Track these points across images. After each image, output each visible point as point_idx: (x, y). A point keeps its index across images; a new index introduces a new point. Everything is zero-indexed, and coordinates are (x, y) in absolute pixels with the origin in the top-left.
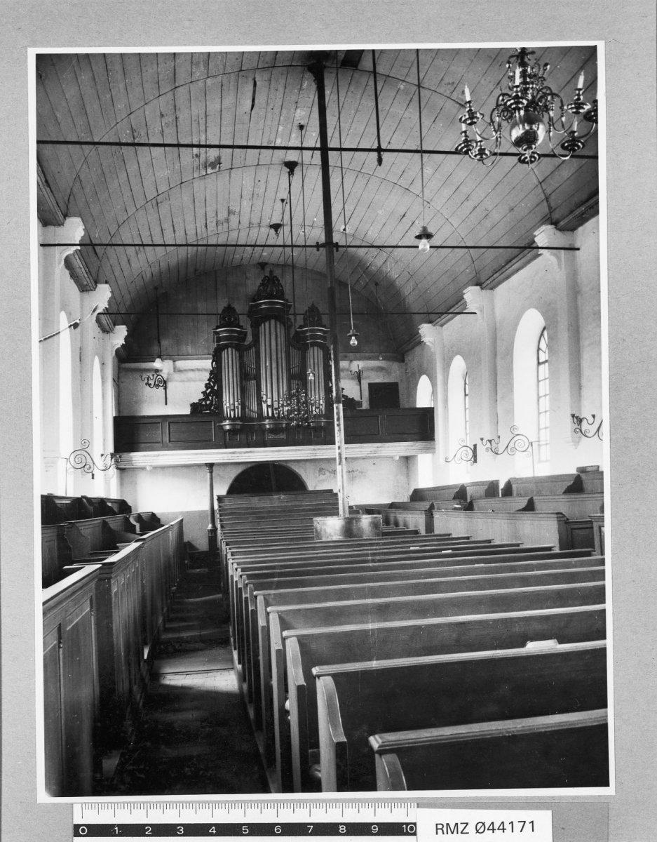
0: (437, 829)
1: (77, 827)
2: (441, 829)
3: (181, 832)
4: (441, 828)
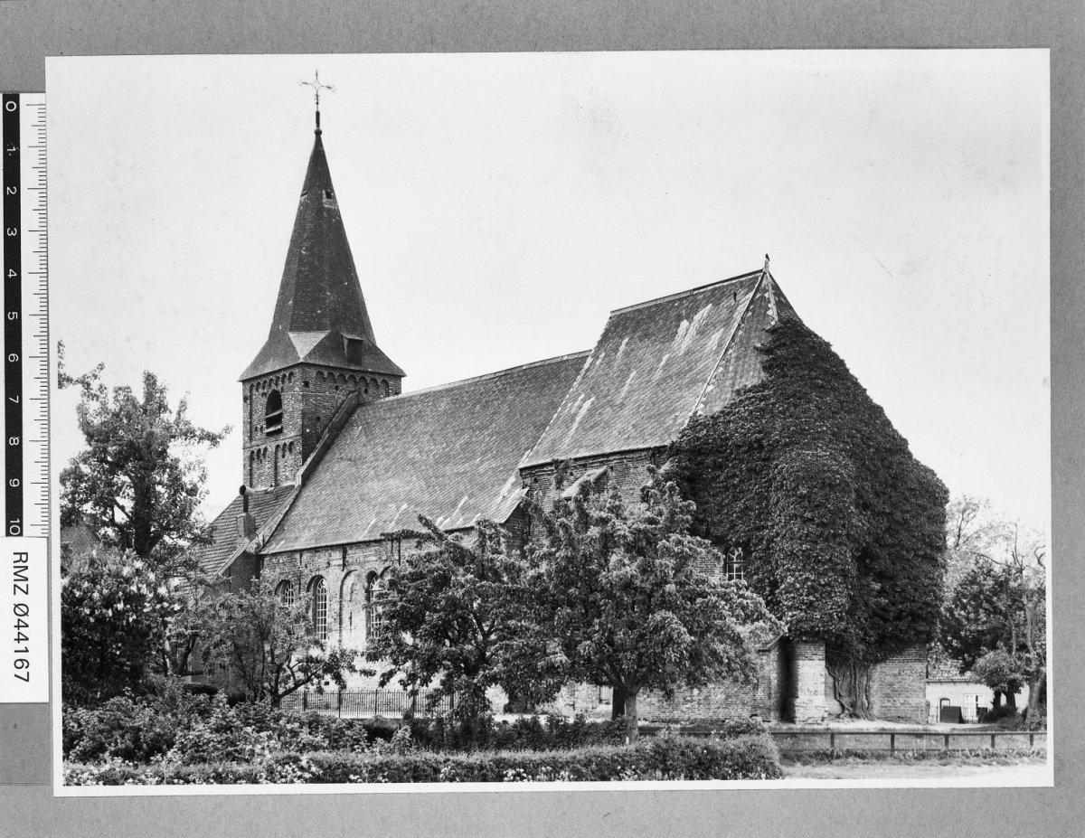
0: (21, 554)
1: (16, 98)
2: (21, 559)
3: (10, 233)
4: (22, 556)
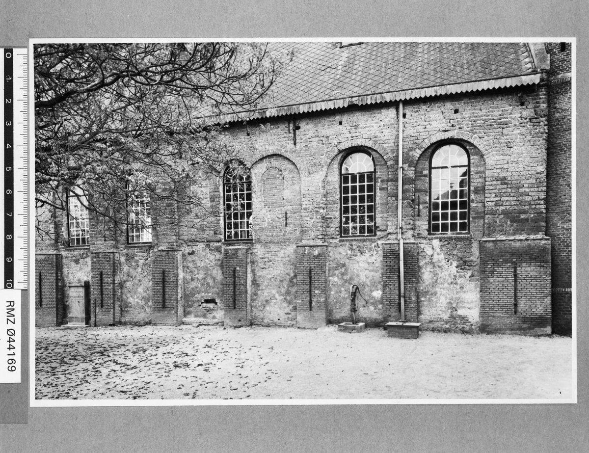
0: (10, 302)
1: (11, 51)
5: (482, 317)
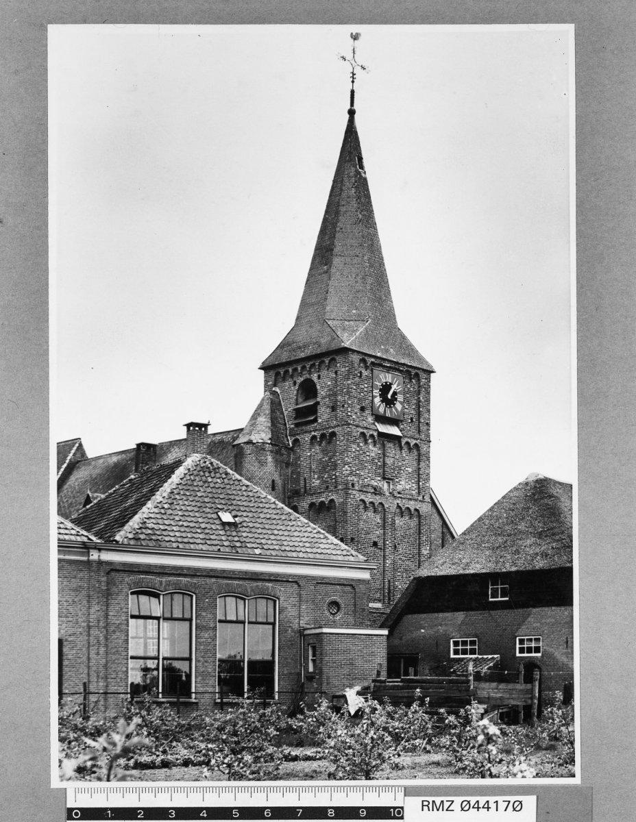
0: (423, 806)
1: (70, 810)
2: (427, 806)
3: (172, 815)
5: (451, 698)
